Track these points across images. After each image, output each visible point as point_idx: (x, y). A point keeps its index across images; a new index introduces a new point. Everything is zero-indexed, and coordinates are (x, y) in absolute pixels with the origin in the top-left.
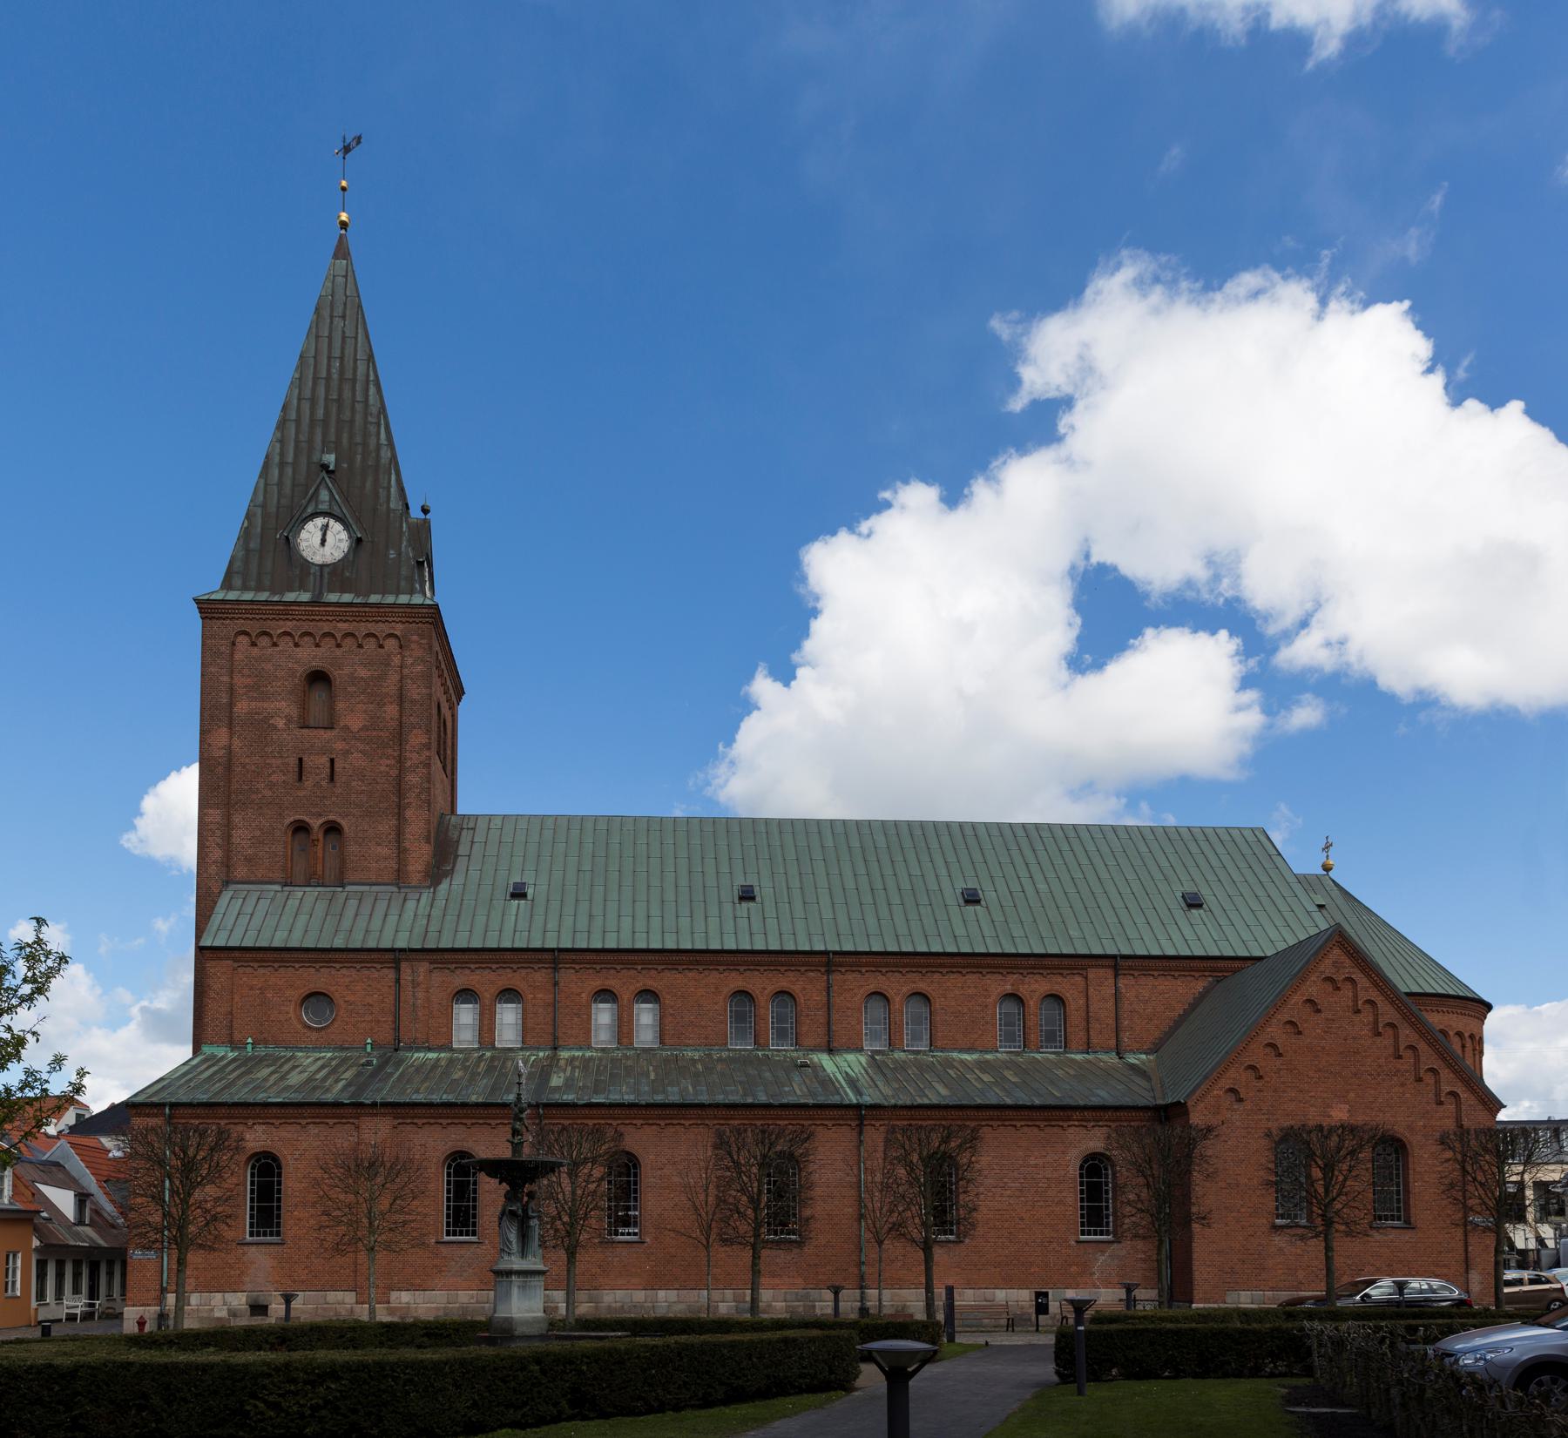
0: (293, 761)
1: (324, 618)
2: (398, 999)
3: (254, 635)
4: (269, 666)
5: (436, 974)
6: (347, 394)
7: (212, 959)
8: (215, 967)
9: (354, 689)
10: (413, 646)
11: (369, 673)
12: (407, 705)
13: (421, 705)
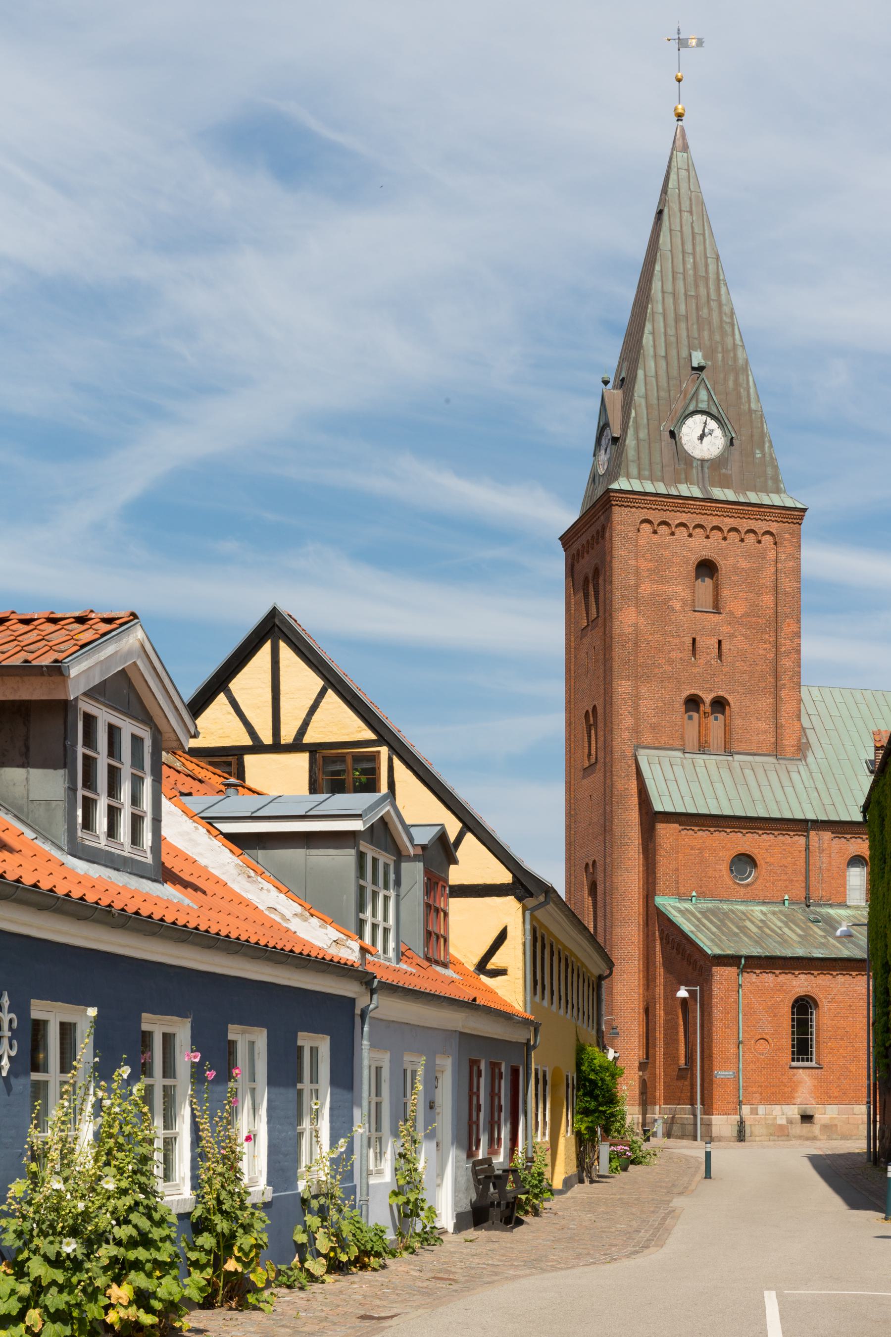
1: (714, 513)
2: (807, 862)
3: (656, 524)
4: (667, 553)
5: (836, 841)
6: (703, 291)
8: (665, 829)
9: (737, 578)
10: (786, 543)
11: (749, 565)
12: (780, 596)
13: (793, 597)
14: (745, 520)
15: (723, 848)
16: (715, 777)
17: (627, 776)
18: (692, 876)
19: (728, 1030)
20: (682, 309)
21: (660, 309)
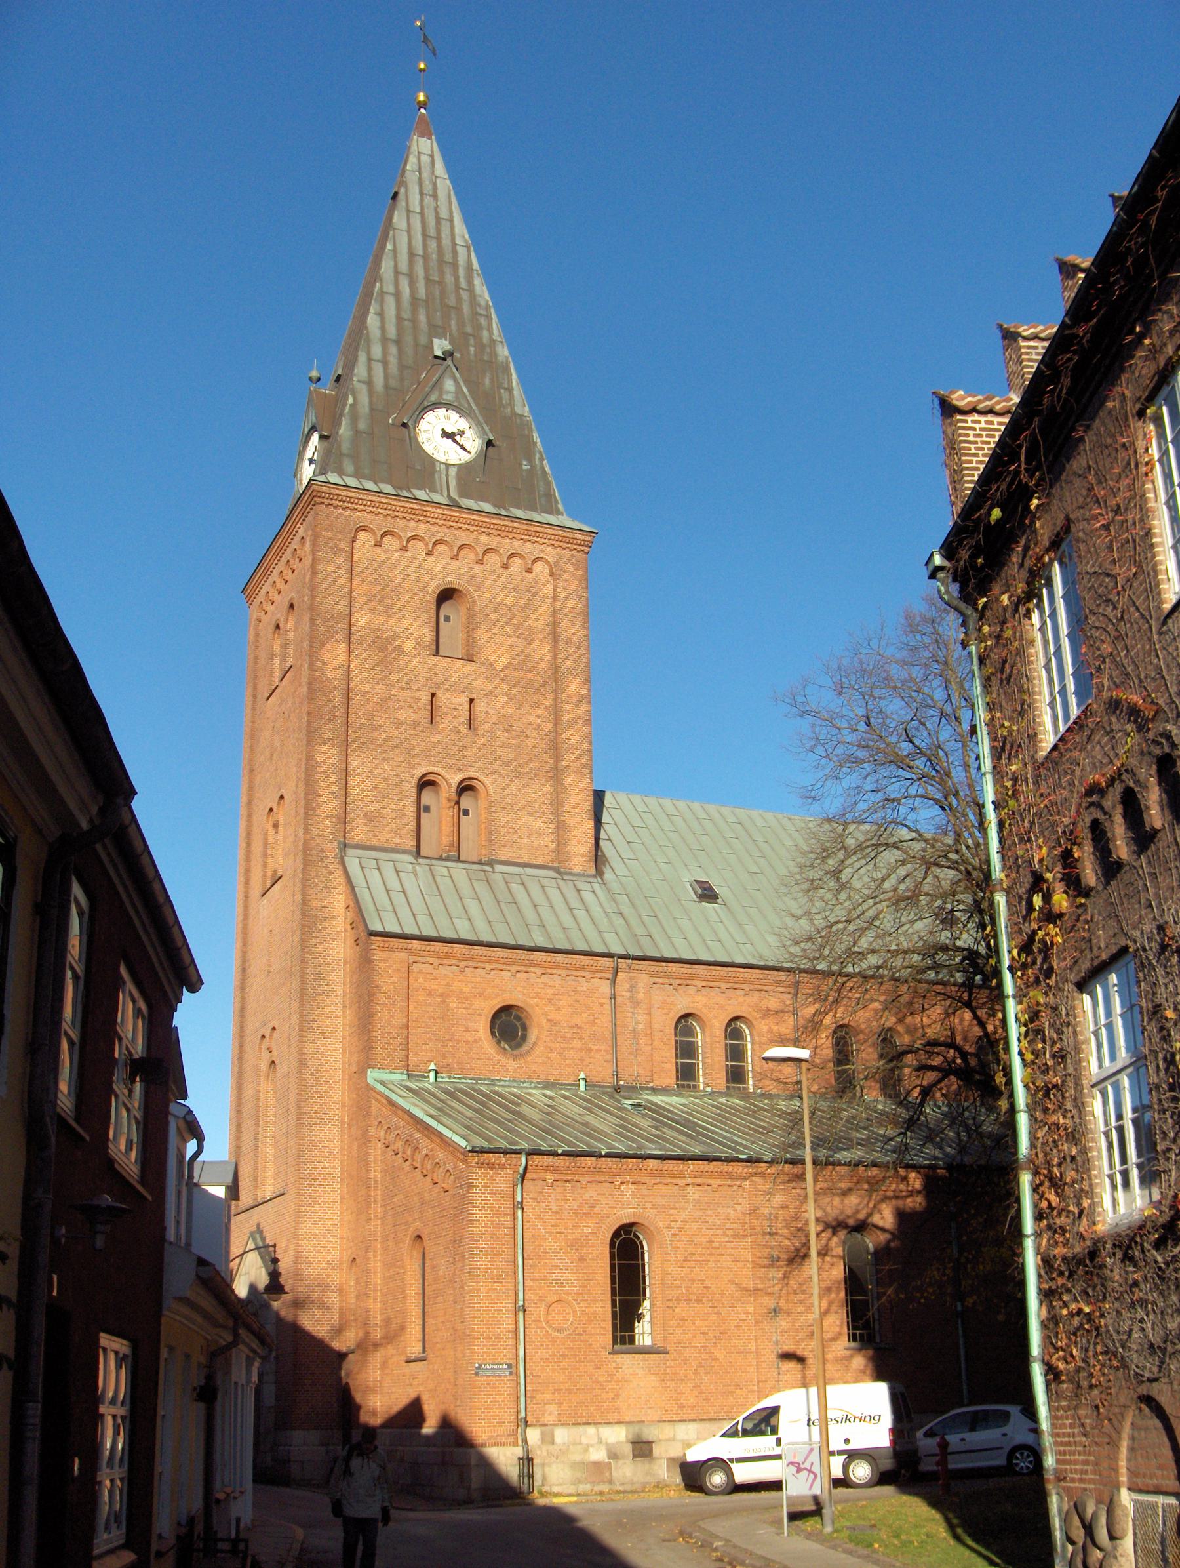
0: (425, 697)
3: (379, 533)
6: (449, 279)
7: (382, 949)
8: (385, 961)
12: (563, 646)
14: (508, 541)
15: (480, 994)
16: (466, 890)
17: (326, 887)
18: (429, 1039)
19: (498, 1287)
20: (422, 292)
21: (391, 289)
